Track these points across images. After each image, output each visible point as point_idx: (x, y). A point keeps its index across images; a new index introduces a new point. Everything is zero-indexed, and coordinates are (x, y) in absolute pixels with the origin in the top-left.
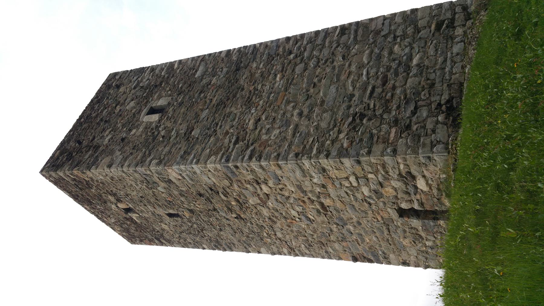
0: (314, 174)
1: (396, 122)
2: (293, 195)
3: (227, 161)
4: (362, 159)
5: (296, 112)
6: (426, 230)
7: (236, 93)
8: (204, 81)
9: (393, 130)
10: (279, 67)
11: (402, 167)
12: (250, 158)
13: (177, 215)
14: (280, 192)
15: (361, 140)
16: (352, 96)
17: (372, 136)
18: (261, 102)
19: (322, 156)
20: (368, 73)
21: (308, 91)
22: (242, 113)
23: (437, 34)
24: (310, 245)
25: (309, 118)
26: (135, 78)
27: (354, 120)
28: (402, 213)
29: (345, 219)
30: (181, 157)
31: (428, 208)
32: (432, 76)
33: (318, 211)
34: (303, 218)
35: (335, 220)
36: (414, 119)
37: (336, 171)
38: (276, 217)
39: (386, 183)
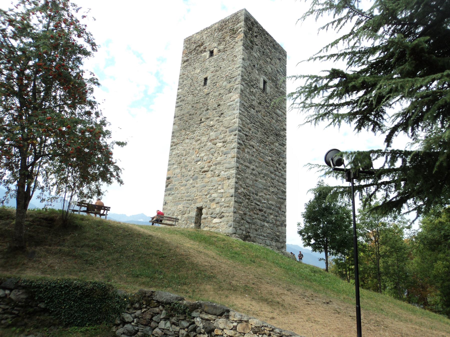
0: (226, 173)
1: (245, 214)
2: (214, 158)
3: (239, 131)
4: (233, 198)
5: (254, 167)
6: (189, 218)
7: (266, 135)
8: (274, 115)
9: (242, 213)
10: (274, 159)
11: (228, 214)
12: (239, 143)
13: (205, 84)
14: (217, 152)
15: (240, 198)
16: (257, 195)
17: (241, 203)
18: (260, 149)
19: (236, 180)
20: (265, 203)
21: (262, 173)
22: (257, 138)
23: (275, 234)
24: (178, 156)
25: (251, 174)
26: (282, 70)
27: (249, 195)
28: (200, 210)
29: (197, 180)
30: (243, 104)
31: (202, 221)
32: (259, 231)
33: (202, 168)
34: (199, 158)
35: (196, 175)
36: (245, 222)
37: (227, 184)
38: (200, 144)
39: (218, 205)
